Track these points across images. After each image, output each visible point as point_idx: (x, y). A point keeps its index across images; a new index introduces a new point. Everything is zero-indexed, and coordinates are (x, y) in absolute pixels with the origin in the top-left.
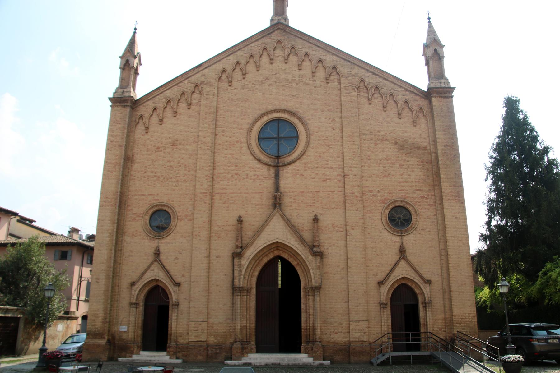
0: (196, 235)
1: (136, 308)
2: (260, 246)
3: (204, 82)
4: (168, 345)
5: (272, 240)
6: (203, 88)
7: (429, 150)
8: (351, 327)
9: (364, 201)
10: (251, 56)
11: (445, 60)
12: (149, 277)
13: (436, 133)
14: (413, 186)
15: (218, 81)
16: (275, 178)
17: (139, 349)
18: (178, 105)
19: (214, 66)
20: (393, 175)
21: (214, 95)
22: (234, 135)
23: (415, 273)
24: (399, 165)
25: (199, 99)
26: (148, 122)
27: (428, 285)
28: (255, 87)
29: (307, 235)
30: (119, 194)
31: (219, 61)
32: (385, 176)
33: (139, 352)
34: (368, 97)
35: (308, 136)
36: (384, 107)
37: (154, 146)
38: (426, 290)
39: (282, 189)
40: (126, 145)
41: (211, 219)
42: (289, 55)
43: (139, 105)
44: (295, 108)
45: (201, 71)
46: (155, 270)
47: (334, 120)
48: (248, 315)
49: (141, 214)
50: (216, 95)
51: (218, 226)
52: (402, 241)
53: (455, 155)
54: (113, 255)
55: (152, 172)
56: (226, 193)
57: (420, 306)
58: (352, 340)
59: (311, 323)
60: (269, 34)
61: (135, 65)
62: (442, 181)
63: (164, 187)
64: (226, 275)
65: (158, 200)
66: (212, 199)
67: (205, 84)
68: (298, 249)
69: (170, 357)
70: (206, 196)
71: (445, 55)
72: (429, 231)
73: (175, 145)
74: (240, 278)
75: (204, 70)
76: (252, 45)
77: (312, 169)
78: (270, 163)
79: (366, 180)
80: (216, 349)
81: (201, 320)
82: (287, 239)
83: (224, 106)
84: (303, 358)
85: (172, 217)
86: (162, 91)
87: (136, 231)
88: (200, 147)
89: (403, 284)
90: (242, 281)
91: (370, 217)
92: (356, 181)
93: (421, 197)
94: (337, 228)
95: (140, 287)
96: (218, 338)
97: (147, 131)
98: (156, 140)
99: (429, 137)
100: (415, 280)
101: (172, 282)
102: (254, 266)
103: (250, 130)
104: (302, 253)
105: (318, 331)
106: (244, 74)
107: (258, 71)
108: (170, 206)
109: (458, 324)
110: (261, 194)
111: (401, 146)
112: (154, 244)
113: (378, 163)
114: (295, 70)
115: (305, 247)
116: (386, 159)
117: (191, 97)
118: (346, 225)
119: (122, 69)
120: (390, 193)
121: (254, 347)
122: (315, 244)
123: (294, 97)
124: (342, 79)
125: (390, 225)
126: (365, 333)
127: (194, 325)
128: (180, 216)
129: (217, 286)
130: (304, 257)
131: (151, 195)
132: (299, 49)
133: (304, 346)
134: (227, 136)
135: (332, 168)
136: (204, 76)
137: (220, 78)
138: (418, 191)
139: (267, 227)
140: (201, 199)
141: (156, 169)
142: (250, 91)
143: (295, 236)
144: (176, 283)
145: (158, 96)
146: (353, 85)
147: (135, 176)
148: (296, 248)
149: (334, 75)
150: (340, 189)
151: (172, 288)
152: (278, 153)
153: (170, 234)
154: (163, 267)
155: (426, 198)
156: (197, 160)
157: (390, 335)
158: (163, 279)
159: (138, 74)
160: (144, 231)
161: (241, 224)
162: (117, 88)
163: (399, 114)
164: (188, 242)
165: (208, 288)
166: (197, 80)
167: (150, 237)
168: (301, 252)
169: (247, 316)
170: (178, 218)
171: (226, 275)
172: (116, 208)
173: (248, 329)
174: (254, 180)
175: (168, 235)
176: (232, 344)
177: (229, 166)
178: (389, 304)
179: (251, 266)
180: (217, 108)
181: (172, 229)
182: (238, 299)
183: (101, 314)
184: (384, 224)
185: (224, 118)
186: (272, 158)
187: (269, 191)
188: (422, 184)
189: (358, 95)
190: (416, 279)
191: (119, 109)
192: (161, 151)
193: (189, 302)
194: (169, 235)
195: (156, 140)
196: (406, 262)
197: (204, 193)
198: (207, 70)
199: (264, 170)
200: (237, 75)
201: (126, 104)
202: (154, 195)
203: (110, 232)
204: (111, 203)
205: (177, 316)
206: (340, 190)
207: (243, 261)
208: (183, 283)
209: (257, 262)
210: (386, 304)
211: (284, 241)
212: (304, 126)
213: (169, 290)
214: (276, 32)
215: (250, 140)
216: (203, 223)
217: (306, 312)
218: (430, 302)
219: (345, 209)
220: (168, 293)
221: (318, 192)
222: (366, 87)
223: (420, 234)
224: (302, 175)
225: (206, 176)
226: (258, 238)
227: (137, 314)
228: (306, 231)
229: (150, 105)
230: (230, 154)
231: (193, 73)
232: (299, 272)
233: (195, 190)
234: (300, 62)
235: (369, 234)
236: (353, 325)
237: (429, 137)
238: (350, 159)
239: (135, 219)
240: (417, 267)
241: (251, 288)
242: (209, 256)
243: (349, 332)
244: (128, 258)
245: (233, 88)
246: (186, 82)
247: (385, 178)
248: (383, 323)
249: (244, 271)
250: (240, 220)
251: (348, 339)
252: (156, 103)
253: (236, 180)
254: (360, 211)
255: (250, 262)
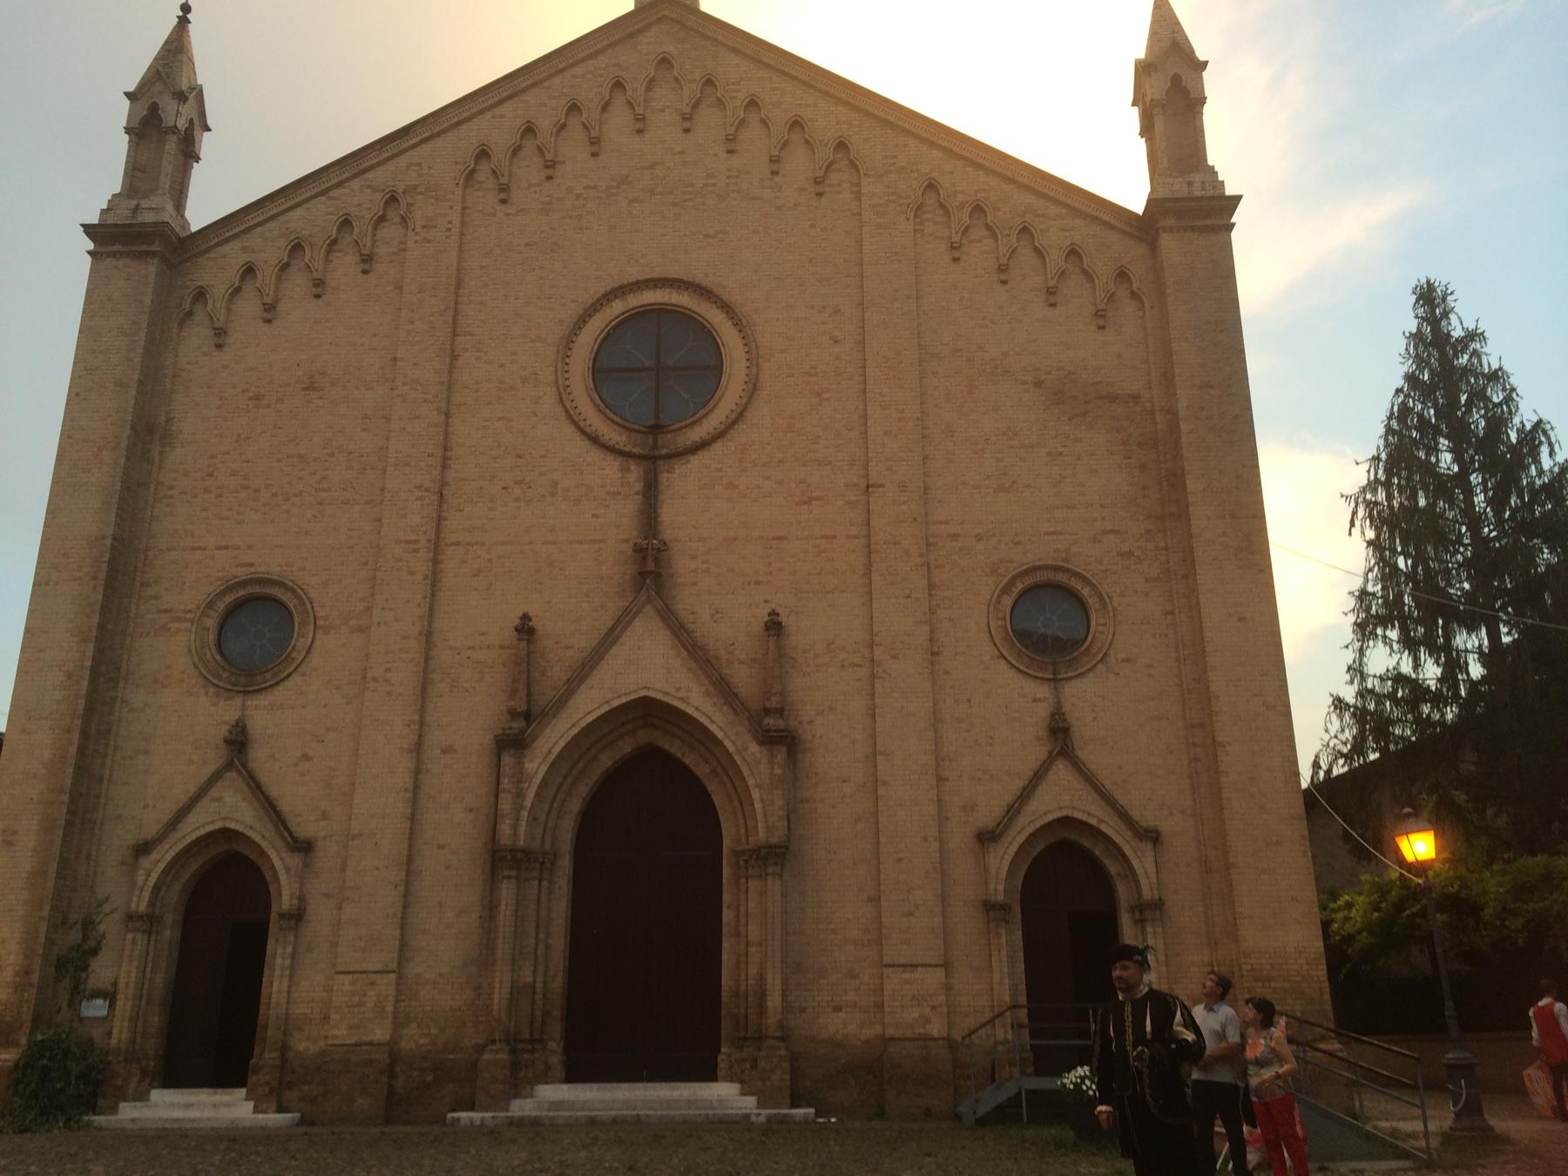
0: (375, 679)
1: (150, 933)
2: (589, 713)
3: (417, 186)
4: (254, 1061)
5: (630, 693)
6: (412, 205)
7: (1147, 404)
8: (888, 987)
9: (932, 566)
10: (574, 108)
11: (1206, 109)
12: (199, 823)
13: (1173, 345)
14: (1095, 520)
15: (466, 187)
16: (644, 496)
17: (148, 1081)
18: (327, 260)
19: (450, 137)
20: (1028, 486)
21: (449, 230)
22: (515, 357)
23: (1103, 804)
24: (1049, 454)
25: (401, 243)
26: (223, 311)
27: (1149, 846)
28: (584, 206)
29: (743, 678)
30: (108, 542)
31: (468, 120)
32: (1001, 489)
33: (149, 1092)
34: (950, 238)
35: (753, 360)
36: (1002, 269)
37: (244, 391)
38: (1143, 862)
39: (667, 533)
40: (140, 382)
41: (430, 627)
42: (696, 105)
43: (195, 256)
44: (714, 274)
45: (407, 150)
46: (226, 800)
47: (837, 312)
48: (541, 947)
49: (190, 611)
50: (456, 230)
51: (451, 648)
52: (1058, 697)
53: (1236, 417)
54: (73, 750)
55: (234, 474)
56: (483, 544)
57: (1124, 920)
58: (890, 1032)
59: (753, 971)
60: (631, 36)
61: (182, 124)
62: (1190, 500)
63: (273, 522)
64: (471, 810)
65: (252, 565)
66: (436, 562)
67: (421, 193)
68: (712, 721)
69: (255, 1106)
70: (416, 551)
71: (1208, 92)
72: (1150, 666)
73: (314, 389)
74: (518, 820)
75: (418, 149)
76: (578, 70)
77: (764, 465)
78: (628, 449)
79: (939, 501)
80: (423, 1070)
81: (379, 967)
82: (678, 689)
83: (482, 267)
84: (724, 1095)
85: (296, 620)
86: (272, 212)
87: (168, 667)
88: (401, 396)
89: (1064, 846)
90: (523, 828)
91: (950, 620)
92: (904, 503)
93: (1119, 554)
94: (843, 656)
95: (168, 858)
96: (433, 1031)
97: (220, 341)
98: (252, 369)
99: (1147, 362)
100: (1104, 828)
101: (282, 837)
102: (569, 780)
103: (568, 343)
104: (725, 734)
105: (774, 1001)
106: (550, 165)
107: (594, 155)
108: (290, 584)
109: (1260, 984)
110: (597, 546)
111: (1055, 394)
112: (228, 711)
113: (980, 447)
114: (715, 155)
115: (736, 713)
116: (1004, 434)
117: (374, 235)
118: (871, 646)
119: (137, 134)
120: (1016, 544)
121: (556, 1060)
122: (768, 705)
123: (711, 240)
124: (865, 181)
125: (1017, 644)
126: (934, 1008)
127: (349, 988)
128: (326, 618)
129: (441, 847)
130: (731, 749)
131: (226, 548)
132: (728, 85)
133: (729, 1056)
134: (490, 362)
135: (830, 463)
136: (416, 168)
137: (470, 175)
138: (1111, 536)
139: (615, 650)
140: (400, 560)
141: (250, 464)
142: (569, 220)
143: (703, 677)
144: (295, 840)
145: (259, 229)
146: (901, 201)
147: (172, 488)
148: (708, 716)
149: (839, 170)
150: (854, 531)
151: (282, 859)
152: (657, 417)
153: (289, 675)
154: (257, 789)
155: (1138, 557)
156: (387, 439)
157: (1023, 1014)
158: (251, 828)
159: (198, 159)
160: (196, 666)
161: (528, 641)
162: (114, 195)
163: (1050, 292)
164: (348, 703)
165: (409, 855)
166: (393, 179)
167: (218, 686)
168: (722, 729)
169: (536, 951)
170: (320, 623)
171: (471, 810)
172: (95, 588)
173: (539, 996)
174: (578, 501)
175: (278, 679)
176: (480, 1049)
177: (494, 458)
178: (1017, 909)
179: (559, 780)
180: (459, 271)
181: (293, 659)
182: (507, 891)
183: (12, 957)
184: (996, 641)
185: (481, 303)
186: (637, 431)
187: (626, 537)
188: (1124, 515)
189: (915, 231)
190: (1108, 825)
191: (121, 263)
192: (269, 406)
193: (340, 908)
194: (283, 680)
195: (252, 369)
196: (1070, 766)
197: (409, 542)
198: (427, 147)
199: (610, 468)
200: (528, 169)
201: (145, 248)
202: (237, 548)
203: (71, 669)
204: (79, 574)
205: (293, 956)
206: (854, 533)
207: (531, 761)
208: (324, 838)
209: (580, 765)
210: (1005, 908)
211: (667, 694)
212: (740, 331)
213: (273, 868)
214: (655, 29)
215: (566, 375)
216: (404, 638)
217: (738, 934)
218: (1158, 905)
219: (871, 593)
220: (268, 876)
221: (782, 538)
222: (942, 205)
223: (1118, 674)
224: (731, 486)
225: (419, 487)
226: (583, 686)
227: (151, 954)
228: (742, 663)
229: (233, 256)
230: (500, 419)
231: (381, 158)
232: (718, 800)
233: (379, 533)
234: (734, 128)
235: (947, 673)
236: (896, 981)
237: (1147, 362)
238: (886, 433)
239: (165, 628)
240: (1108, 785)
241: (555, 855)
242: (418, 749)
243: (880, 1006)
244: (132, 758)
245: (512, 211)
246: (356, 184)
247: (1000, 494)
248: (996, 976)
249: (530, 796)
250: (525, 629)
251: (876, 1030)
252: (253, 251)
253: (517, 500)
254: (918, 600)
255: (552, 764)
